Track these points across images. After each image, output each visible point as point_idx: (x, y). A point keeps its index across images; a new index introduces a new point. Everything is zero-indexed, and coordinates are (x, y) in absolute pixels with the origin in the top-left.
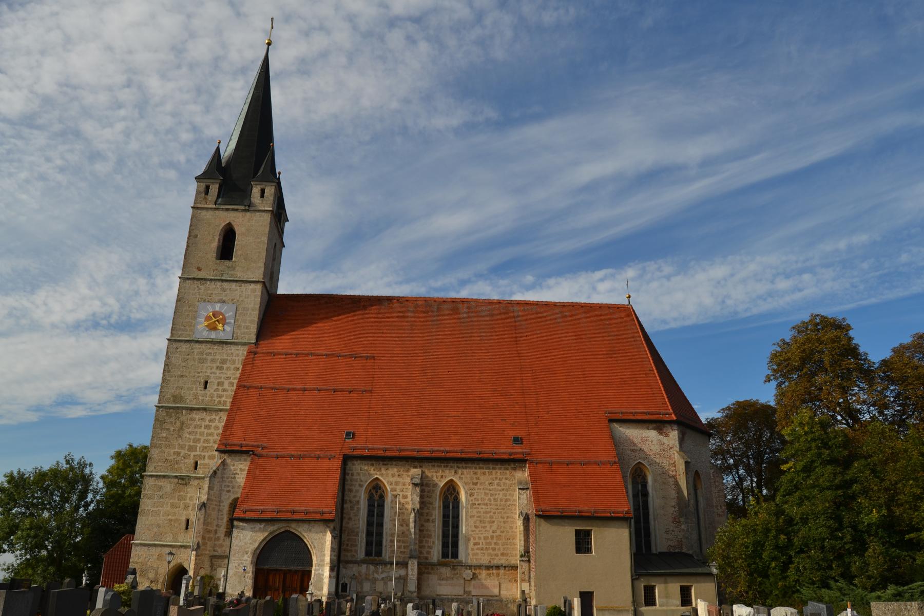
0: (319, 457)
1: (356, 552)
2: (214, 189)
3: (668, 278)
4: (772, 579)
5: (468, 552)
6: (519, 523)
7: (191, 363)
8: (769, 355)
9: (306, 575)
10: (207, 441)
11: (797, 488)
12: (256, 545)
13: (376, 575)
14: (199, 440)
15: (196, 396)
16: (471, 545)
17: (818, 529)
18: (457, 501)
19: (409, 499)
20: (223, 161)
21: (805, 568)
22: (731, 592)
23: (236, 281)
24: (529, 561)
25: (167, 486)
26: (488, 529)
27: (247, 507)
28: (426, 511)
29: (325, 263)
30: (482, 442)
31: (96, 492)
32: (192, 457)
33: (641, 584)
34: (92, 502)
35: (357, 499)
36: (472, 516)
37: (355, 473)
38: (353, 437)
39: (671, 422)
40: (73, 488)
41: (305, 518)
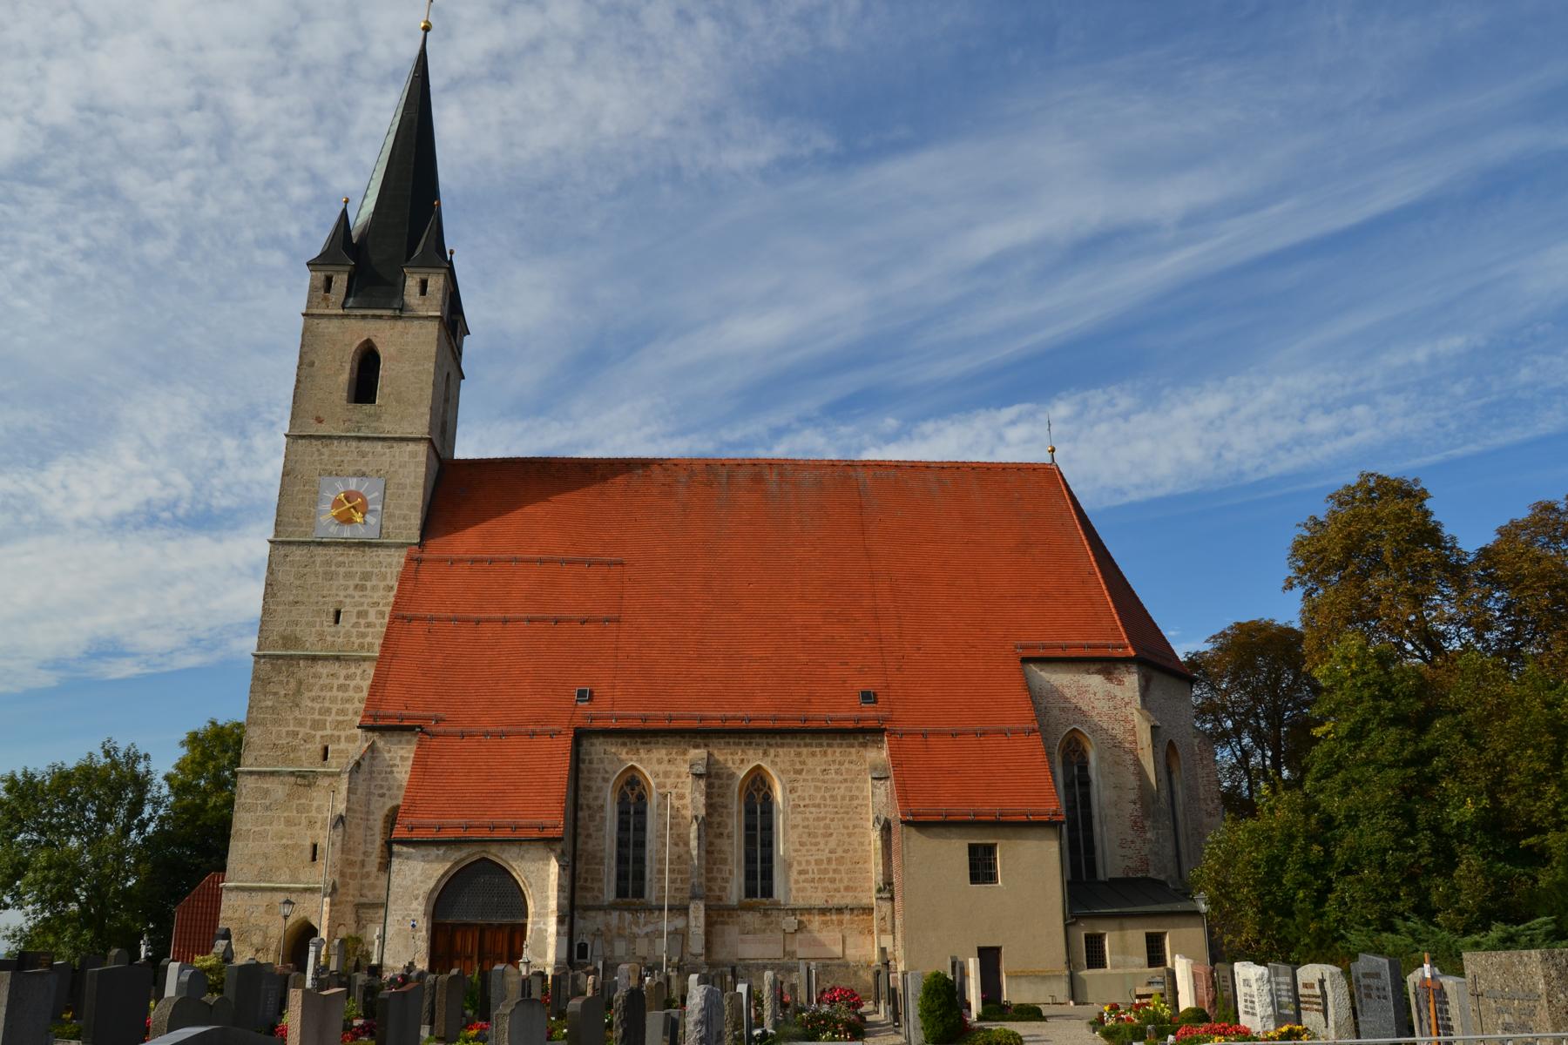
0: (534, 734)
1: (601, 891)
2: (341, 281)
3: (1126, 416)
4: (1299, 919)
5: (790, 887)
6: (875, 836)
8: (1290, 543)
10: (342, 712)
11: (1339, 766)
12: (432, 884)
13: (635, 929)
14: (329, 711)
15: (321, 636)
16: (794, 875)
17: (1374, 833)
19: (688, 800)
20: (355, 234)
21: (1354, 900)
22: (1231, 942)
23: (379, 439)
24: (892, 899)
25: (278, 789)
26: (822, 846)
27: (414, 821)
28: (716, 819)
29: (541, 405)
30: (809, 701)
31: (157, 803)
33: (1081, 933)
35: (600, 802)
36: (794, 827)
37: (595, 757)
38: (591, 699)
39: (1126, 661)
41: (512, 836)
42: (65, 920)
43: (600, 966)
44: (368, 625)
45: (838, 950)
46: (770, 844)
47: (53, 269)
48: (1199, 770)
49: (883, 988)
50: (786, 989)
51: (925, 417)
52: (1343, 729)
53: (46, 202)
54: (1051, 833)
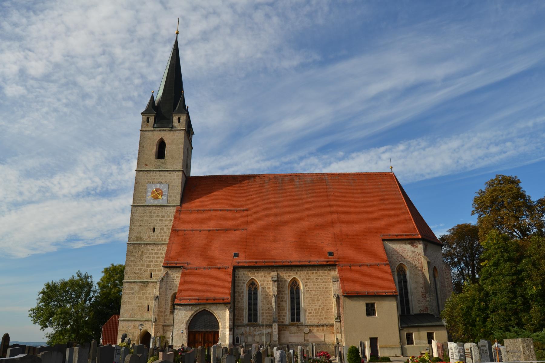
0: (220, 268)
1: (243, 320)
2: (152, 119)
3: (424, 149)
4: (477, 327)
5: (306, 318)
6: (334, 300)
7: (145, 218)
8: (473, 199)
9: (216, 334)
10: (156, 261)
11: (490, 275)
12: (188, 318)
13: (255, 333)
14: (152, 261)
16: (307, 314)
17: (502, 298)
18: (298, 289)
19: (271, 289)
20: (156, 103)
21: (496, 321)
22: (455, 335)
23: (168, 171)
24: (340, 322)
25: (136, 287)
26: (316, 304)
27: (182, 298)
28: (281, 296)
29: (220, 151)
30: (311, 255)
31: (95, 292)
32: (149, 271)
33: (405, 332)
34: (93, 297)
35: (242, 290)
36: (307, 298)
37: (240, 276)
38: (238, 256)
39: (418, 240)
40: (83, 290)
41: (214, 302)
42: (66, 331)
43: (244, 345)
44: (164, 231)
45: (323, 339)
46: (299, 304)
47: (56, 110)
48: (445, 276)
49: (337, 352)
50: (305, 351)
51: (353, 151)
52: (491, 262)
53: (53, 88)
54: (394, 299)
